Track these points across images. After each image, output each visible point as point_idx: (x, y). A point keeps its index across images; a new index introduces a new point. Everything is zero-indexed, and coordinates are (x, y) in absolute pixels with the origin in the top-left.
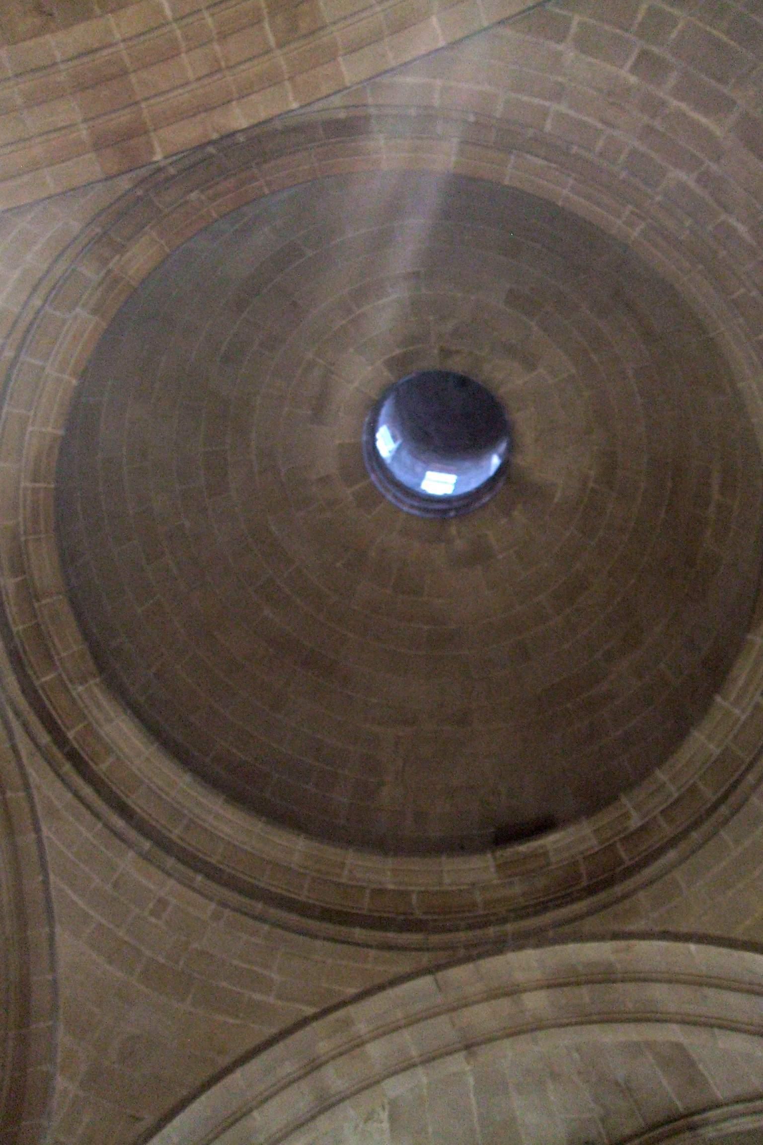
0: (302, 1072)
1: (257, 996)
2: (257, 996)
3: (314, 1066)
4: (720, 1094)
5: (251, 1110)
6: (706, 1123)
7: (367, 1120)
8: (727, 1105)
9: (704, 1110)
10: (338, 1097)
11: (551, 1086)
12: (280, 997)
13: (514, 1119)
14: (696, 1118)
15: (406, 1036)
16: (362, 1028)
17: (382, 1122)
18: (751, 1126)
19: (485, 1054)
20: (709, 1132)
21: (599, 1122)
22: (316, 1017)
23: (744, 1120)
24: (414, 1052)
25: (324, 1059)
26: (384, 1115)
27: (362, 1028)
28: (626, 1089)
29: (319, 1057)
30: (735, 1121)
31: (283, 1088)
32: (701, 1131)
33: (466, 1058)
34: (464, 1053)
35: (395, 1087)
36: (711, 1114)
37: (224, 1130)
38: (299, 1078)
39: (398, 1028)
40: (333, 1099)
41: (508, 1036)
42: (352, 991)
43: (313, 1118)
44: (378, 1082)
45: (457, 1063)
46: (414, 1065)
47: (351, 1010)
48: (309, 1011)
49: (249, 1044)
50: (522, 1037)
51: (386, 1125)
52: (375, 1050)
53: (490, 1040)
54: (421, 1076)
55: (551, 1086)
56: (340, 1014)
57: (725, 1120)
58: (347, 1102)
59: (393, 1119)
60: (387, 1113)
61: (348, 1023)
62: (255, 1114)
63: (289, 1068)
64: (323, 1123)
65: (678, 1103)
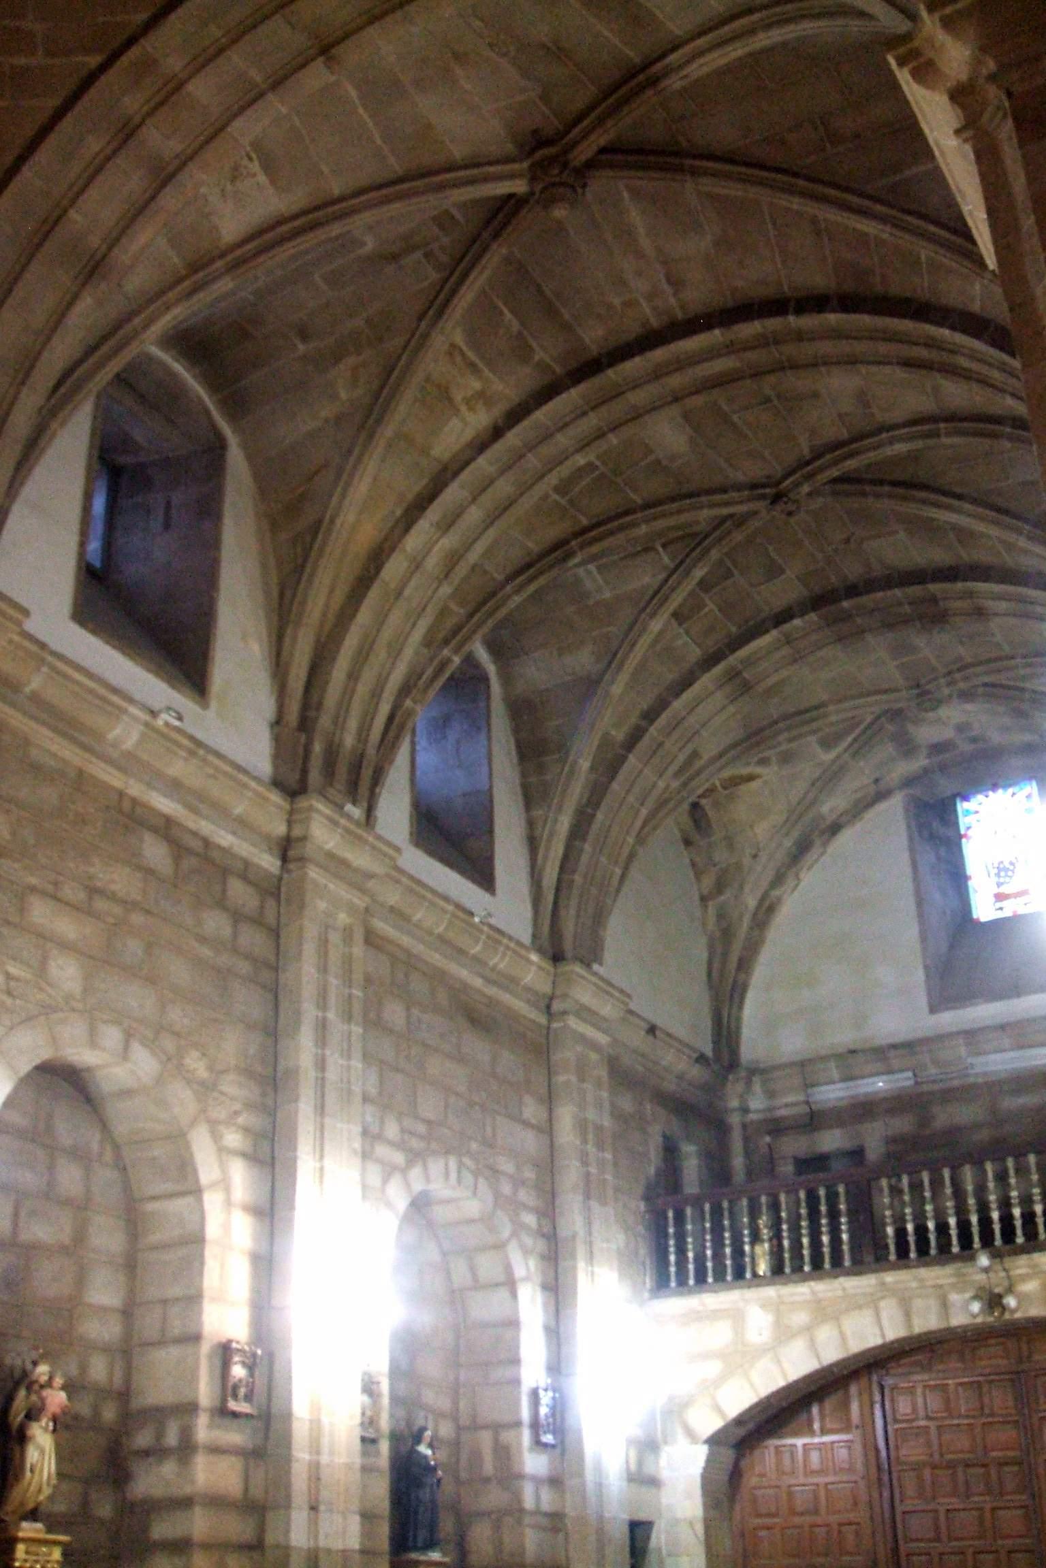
0: (115, 144)
1: (22, 61)
2: (22, 61)
3: (128, 132)
4: (677, 27)
5: (65, 211)
6: (667, 72)
7: (233, 179)
8: (692, 39)
9: (664, 55)
10: (177, 162)
11: (459, 71)
12: (50, 53)
13: (429, 126)
14: (658, 66)
15: (236, 59)
16: (174, 64)
17: (254, 175)
18: (723, 61)
19: (351, 53)
20: (675, 83)
21: (540, 104)
22: (103, 68)
23: (709, 57)
24: (256, 76)
25: (137, 119)
26: (255, 167)
27: (174, 64)
28: (557, 51)
29: (130, 119)
30: (702, 61)
31: (99, 169)
32: (664, 83)
33: (325, 63)
34: (321, 59)
35: (246, 129)
36: (673, 58)
37: (40, 245)
38: (115, 152)
39: (221, 51)
40: (171, 168)
41: (371, 22)
42: (141, 17)
43: (153, 198)
44: (222, 129)
45: (317, 76)
46: (262, 95)
47: (149, 45)
48: (94, 61)
49: (29, 130)
50: (389, 19)
51: (262, 178)
52: (201, 89)
53: (347, 36)
54: (277, 105)
55: (459, 71)
56: (134, 53)
57: (688, 62)
58: (191, 165)
59: (268, 166)
60: (256, 163)
61: (149, 65)
62: (73, 214)
63: (94, 145)
64: (169, 200)
65: (632, 54)
